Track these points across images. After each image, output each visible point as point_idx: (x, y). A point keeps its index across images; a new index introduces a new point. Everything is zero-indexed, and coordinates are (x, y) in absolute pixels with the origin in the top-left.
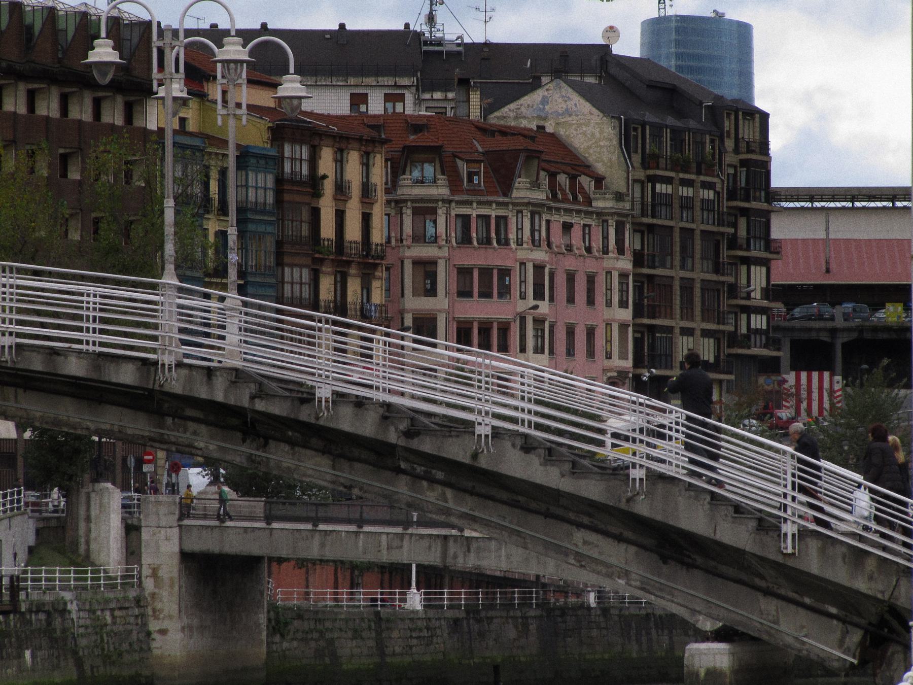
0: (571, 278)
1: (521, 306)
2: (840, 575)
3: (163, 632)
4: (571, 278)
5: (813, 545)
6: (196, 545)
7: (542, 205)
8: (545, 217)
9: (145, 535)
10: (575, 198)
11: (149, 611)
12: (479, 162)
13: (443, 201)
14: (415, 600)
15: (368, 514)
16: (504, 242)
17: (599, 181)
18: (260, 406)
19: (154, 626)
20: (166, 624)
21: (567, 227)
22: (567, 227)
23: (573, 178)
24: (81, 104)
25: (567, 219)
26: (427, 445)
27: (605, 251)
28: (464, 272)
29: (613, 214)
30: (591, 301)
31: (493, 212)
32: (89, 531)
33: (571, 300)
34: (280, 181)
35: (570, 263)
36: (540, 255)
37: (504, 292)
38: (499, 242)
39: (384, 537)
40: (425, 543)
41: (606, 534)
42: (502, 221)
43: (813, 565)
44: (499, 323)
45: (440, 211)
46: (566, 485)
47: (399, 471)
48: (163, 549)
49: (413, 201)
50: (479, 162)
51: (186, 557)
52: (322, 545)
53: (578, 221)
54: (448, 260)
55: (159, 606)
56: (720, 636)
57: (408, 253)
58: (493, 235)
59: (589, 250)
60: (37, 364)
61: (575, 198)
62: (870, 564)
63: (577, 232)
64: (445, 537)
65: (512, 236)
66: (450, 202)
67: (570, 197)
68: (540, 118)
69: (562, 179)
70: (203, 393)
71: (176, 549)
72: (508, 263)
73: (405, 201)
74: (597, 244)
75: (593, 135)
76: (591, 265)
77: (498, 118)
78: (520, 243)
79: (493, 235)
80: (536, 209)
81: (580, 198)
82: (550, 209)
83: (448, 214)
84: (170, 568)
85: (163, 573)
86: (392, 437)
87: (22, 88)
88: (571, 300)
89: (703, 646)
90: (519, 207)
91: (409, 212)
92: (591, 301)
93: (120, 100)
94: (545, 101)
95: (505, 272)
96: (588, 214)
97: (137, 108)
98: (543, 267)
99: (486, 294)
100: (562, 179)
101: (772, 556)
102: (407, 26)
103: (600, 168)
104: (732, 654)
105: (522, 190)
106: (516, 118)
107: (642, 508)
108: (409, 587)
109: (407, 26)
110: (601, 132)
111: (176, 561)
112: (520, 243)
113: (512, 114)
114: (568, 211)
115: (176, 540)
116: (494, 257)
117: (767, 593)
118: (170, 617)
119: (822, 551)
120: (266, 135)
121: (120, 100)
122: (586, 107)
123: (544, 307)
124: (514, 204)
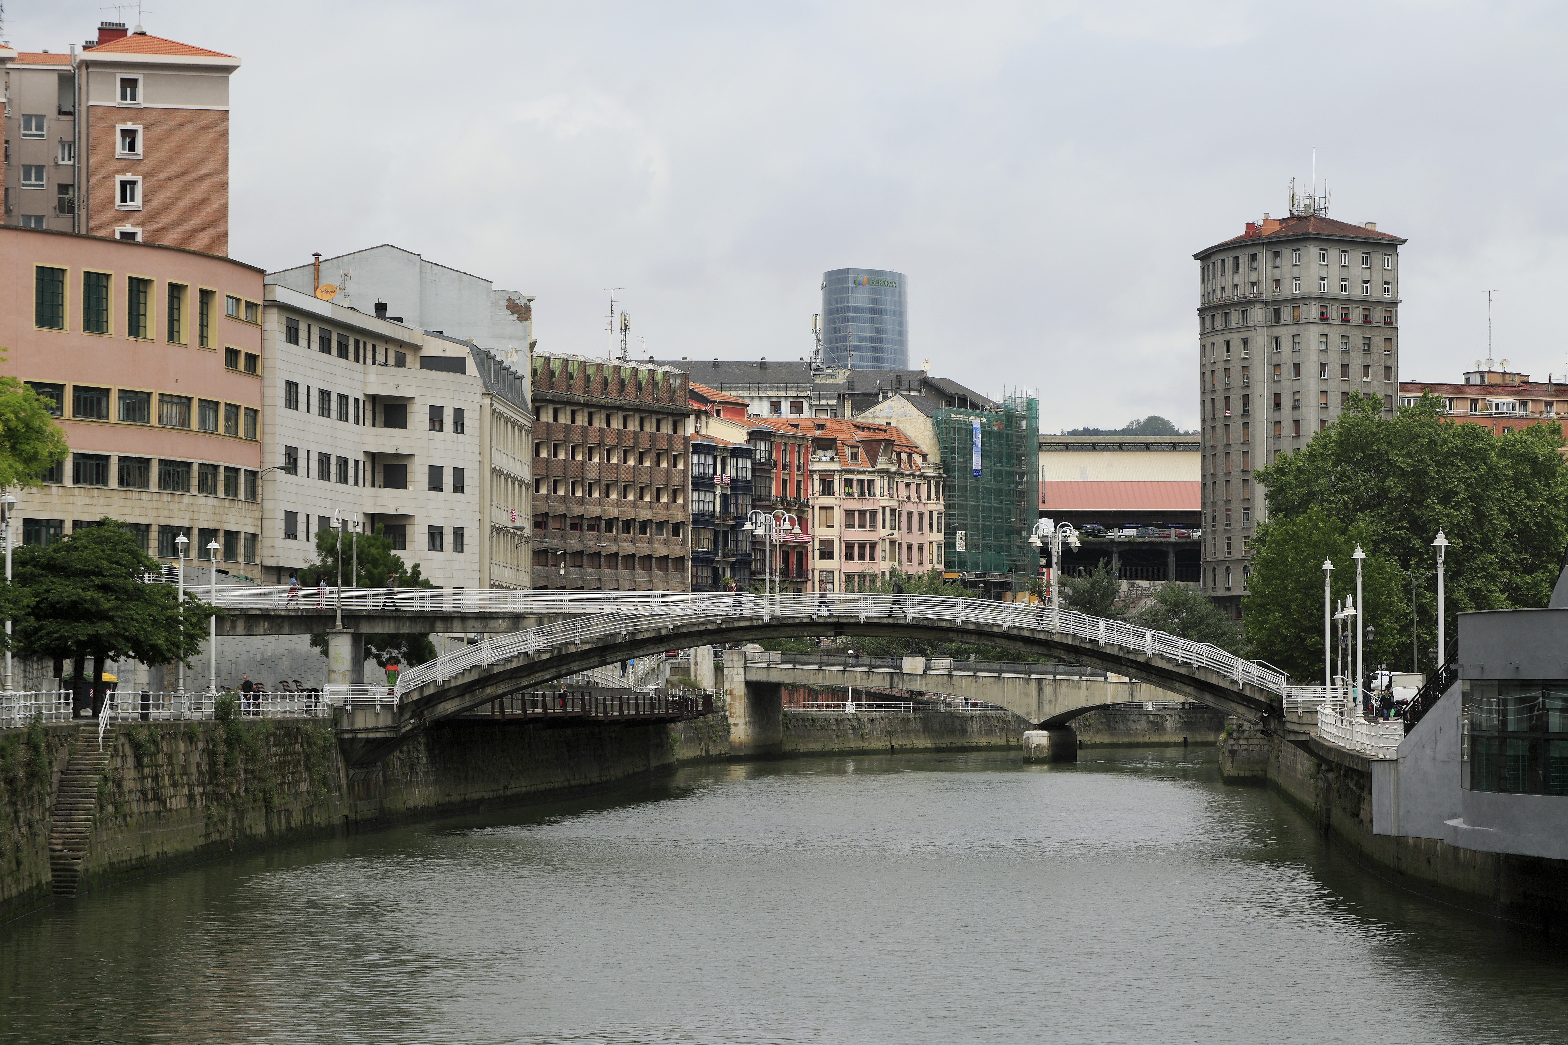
0: (910, 514)
1: (883, 533)
2: (1257, 696)
3: (736, 725)
4: (910, 514)
5: (1248, 687)
6: (754, 677)
7: (894, 473)
8: (896, 479)
9: (726, 672)
10: (911, 467)
11: (728, 714)
12: (858, 447)
13: (838, 471)
14: (850, 708)
15: (799, 658)
16: (872, 495)
17: (924, 457)
18: (1082, 645)
19: (731, 721)
20: (737, 721)
21: (908, 485)
22: (908, 485)
23: (910, 456)
24: (651, 422)
25: (908, 480)
26: (1131, 657)
27: (929, 498)
28: (849, 513)
29: (933, 477)
30: (921, 529)
31: (866, 477)
32: (696, 670)
33: (910, 528)
34: (753, 464)
35: (909, 507)
36: (895, 504)
37: (873, 525)
38: (869, 495)
39: (858, 674)
40: (881, 676)
41: (1185, 684)
42: (871, 482)
43: (1248, 693)
44: (870, 544)
45: (835, 477)
46: (1175, 669)
47: (1122, 664)
48: (735, 680)
49: (820, 471)
50: (858, 447)
51: (749, 684)
52: (824, 678)
53: (914, 482)
54: (840, 506)
55: (734, 710)
56: (1042, 726)
57: (816, 502)
58: (866, 491)
59: (919, 498)
60: (1015, 632)
61: (911, 467)
62: (1265, 693)
63: (913, 487)
64: (892, 674)
65: (877, 491)
66: (841, 471)
67: (908, 466)
68: (887, 417)
69: (904, 456)
70: (1065, 641)
71: (743, 680)
72: (875, 508)
73: (815, 471)
74: (924, 494)
75: (920, 428)
76: (921, 508)
77: (863, 418)
78: (882, 495)
79: (866, 491)
80: (891, 475)
81: (914, 467)
82: (898, 474)
83: (840, 479)
84: (740, 690)
85: (736, 692)
86: (1121, 654)
87: (621, 414)
88: (910, 528)
89: (1036, 732)
90: (881, 473)
91: (817, 477)
92: (921, 529)
93: (670, 420)
94: (890, 407)
95: (873, 513)
96: (920, 477)
97: (679, 425)
98: (895, 510)
99: (863, 526)
100: (904, 456)
101: (1236, 690)
102: (802, 359)
103: (925, 449)
104: (1050, 737)
105: (882, 465)
106: (874, 417)
107: (1196, 676)
108: (847, 701)
109: (802, 359)
110: (925, 427)
111: (743, 686)
112: (882, 495)
113: (871, 415)
114: (908, 475)
115: (743, 676)
116: (868, 505)
117: (1233, 701)
118: (740, 717)
119: (1251, 689)
120: (746, 437)
121: (670, 420)
122: (915, 411)
123: (896, 535)
124: (879, 472)
